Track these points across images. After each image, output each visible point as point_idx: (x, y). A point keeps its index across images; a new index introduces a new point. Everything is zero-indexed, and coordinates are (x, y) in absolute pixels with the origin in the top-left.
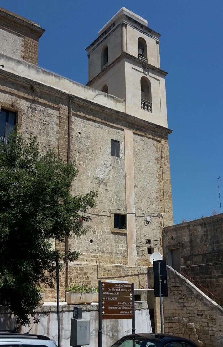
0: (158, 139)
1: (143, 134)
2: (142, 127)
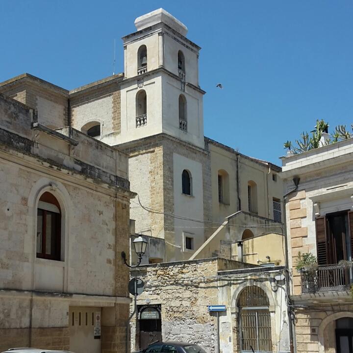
0: (152, 150)
1: (136, 153)
2: (135, 147)
